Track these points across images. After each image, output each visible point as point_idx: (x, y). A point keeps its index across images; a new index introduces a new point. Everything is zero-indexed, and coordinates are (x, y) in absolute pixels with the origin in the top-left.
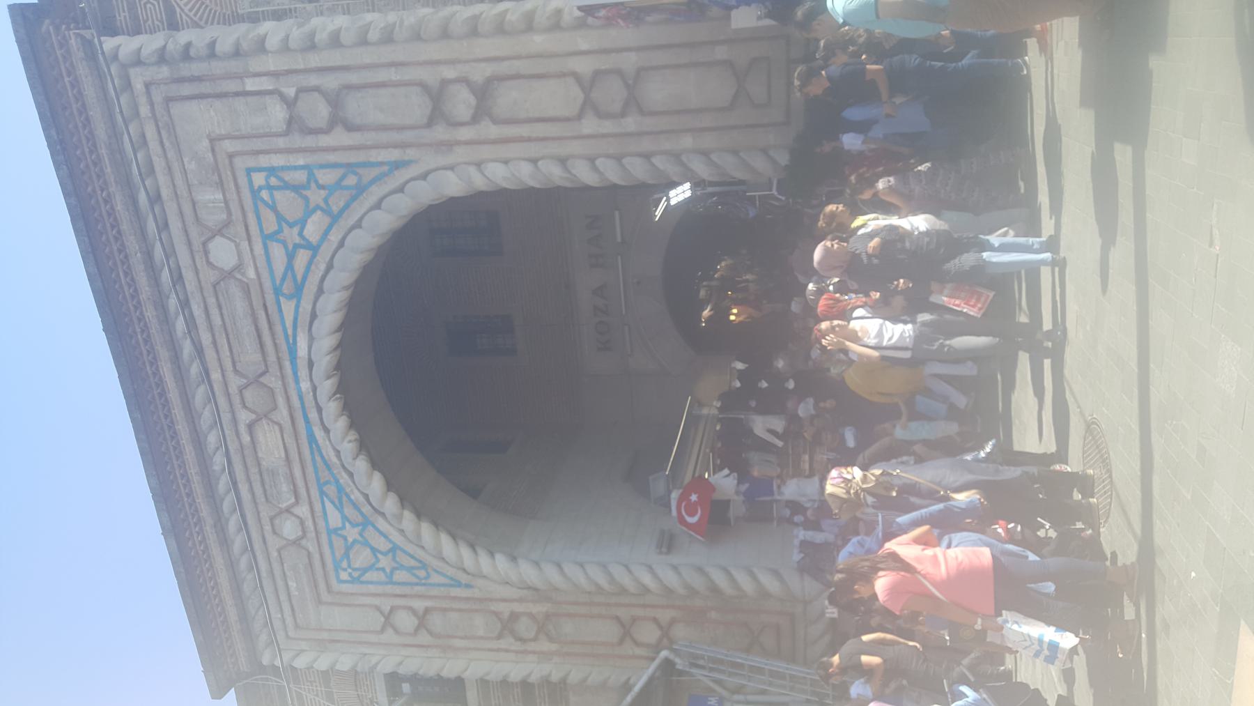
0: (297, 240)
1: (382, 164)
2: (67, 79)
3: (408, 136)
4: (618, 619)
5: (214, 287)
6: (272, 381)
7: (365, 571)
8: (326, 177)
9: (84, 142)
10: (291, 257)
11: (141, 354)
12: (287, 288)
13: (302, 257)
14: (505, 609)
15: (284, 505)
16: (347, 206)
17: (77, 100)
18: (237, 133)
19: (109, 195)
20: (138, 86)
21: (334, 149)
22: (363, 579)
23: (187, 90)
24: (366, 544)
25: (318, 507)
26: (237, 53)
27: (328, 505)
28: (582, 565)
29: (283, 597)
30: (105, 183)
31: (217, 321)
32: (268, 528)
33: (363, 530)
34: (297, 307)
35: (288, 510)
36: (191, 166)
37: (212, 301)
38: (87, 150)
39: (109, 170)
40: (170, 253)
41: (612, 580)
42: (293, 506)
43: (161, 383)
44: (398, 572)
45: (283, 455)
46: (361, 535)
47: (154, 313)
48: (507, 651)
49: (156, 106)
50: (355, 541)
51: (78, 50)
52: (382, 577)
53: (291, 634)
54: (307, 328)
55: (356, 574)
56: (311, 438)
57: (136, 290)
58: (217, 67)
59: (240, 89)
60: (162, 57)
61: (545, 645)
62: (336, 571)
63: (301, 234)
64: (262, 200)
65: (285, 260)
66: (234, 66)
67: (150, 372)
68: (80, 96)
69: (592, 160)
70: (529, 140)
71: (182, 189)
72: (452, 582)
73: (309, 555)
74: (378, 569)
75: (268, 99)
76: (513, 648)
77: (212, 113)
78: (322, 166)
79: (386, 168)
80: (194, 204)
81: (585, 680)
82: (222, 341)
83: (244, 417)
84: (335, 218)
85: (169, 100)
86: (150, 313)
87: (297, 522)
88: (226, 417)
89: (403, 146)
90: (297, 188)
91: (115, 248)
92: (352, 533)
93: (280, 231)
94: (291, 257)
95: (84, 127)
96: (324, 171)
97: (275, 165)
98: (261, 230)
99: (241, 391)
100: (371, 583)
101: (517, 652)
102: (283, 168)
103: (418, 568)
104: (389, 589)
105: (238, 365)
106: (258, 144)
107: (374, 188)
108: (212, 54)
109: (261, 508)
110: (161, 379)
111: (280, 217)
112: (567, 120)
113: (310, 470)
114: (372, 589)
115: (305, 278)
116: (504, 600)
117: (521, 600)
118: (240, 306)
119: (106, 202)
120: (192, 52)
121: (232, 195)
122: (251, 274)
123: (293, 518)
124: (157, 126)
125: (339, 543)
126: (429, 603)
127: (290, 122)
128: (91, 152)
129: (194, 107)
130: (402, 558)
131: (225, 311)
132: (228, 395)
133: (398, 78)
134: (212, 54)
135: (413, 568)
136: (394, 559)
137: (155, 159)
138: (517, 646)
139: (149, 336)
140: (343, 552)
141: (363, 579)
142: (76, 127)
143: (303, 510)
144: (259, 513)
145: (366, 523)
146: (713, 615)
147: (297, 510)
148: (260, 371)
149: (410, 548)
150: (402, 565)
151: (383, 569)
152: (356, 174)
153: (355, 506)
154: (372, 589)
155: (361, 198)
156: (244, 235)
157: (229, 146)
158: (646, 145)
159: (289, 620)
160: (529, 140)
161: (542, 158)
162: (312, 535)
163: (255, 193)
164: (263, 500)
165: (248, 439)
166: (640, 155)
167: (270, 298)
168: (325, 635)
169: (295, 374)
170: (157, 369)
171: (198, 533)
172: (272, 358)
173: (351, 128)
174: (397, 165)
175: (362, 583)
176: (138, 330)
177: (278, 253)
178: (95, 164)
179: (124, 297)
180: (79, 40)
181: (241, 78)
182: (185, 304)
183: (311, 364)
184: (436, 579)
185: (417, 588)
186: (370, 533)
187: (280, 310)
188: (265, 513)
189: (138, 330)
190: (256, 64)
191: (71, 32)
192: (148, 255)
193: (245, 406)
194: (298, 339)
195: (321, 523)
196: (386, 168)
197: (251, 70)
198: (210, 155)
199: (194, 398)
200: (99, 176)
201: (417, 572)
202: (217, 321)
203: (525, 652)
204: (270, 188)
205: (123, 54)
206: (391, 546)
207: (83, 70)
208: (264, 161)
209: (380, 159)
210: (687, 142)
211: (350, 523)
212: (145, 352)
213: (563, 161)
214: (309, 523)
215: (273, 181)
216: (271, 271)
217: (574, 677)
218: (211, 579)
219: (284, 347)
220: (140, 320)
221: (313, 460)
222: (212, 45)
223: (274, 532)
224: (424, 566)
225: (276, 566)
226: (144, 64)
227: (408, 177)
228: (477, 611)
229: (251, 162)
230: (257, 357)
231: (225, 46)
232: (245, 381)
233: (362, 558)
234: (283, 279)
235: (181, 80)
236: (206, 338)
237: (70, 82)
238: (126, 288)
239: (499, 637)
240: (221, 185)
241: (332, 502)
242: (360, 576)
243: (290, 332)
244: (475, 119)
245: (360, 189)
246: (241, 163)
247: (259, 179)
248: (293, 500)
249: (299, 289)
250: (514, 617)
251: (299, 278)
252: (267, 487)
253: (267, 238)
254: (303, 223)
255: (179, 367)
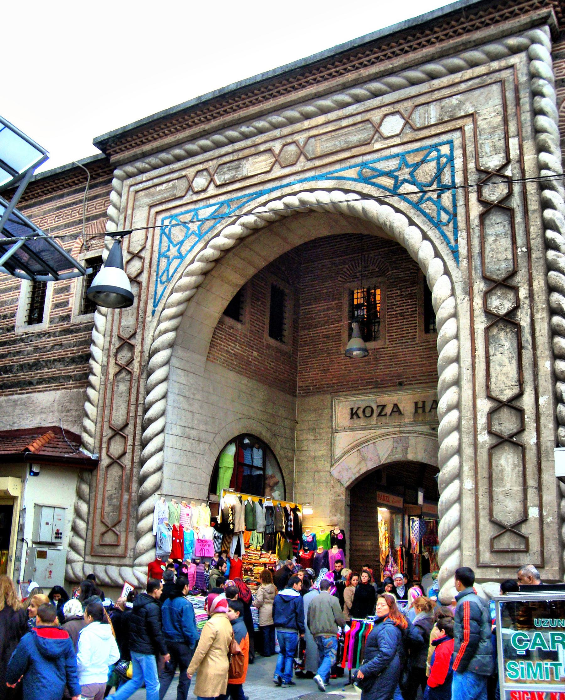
0: (401, 178)
1: (456, 241)
2: (516, 8)
3: (477, 262)
4: (126, 425)
5: (368, 120)
6: (302, 164)
7: (169, 238)
8: (446, 198)
9: (471, 23)
10: (388, 174)
11: (321, 72)
12: (367, 172)
13: (388, 182)
14: (136, 342)
15: (216, 178)
16: (425, 215)
17: (501, 16)
18: (478, 133)
19: (433, 43)
20: (514, 60)
21: (467, 205)
22: (164, 236)
23: (510, 95)
24: (186, 237)
25: (212, 201)
26: (537, 131)
27: (213, 209)
28: (164, 396)
29: (156, 181)
30: (442, 40)
31: (345, 123)
32: (200, 167)
33: (196, 234)
34: (353, 180)
35: (212, 180)
36: (454, 101)
37: (359, 118)
38: (465, 25)
39: (451, 42)
40: (394, 88)
41: (151, 421)
42: (215, 184)
43: (302, 87)
44: (166, 260)
45: (249, 174)
46: (192, 233)
47: (350, 79)
48: (110, 342)
49: (498, 73)
50: (188, 229)
51: (539, 15)
52: (164, 249)
53: (132, 189)
54: (337, 187)
55: (167, 231)
56: (261, 194)
57: (366, 66)
58: (526, 116)
59: (511, 134)
60: (534, 75)
61: (112, 370)
62: (169, 217)
63: (405, 181)
64: (430, 153)
65: (387, 170)
66: (528, 130)
67: (309, 79)
68: (505, 18)
69: (457, 406)
70: (473, 357)
71: (436, 95)
72: (157, 301)
73: (181, 197)
74: (169, 246)
75: (502, 155)
76: (112, 347)
77: (493, 114)
78: (454, 196)
79: (453, 243)
80: (428, 103)
81: (89, 400)
82: (330, 128)
83: (277, 146)
84: (416, 206)
85: (502, 82)
86: (350, 77)
87: (204, 187)
88: (277, 133)
89: (470, 257)
90: (438, 177)
91: (395, 49)
92: (194, 227)
93: (408, 166)
94: (388, 174)
95: (482, 23)
96: (451, 197)
97: (455, 161)
98: (408, 152)
99: (294, 142)
100: (161, 242)
101: (109, 350)
102: (453, 166)
103: (168, 275)
104: (156, 255)
105: (313, 140)
106: (470, 149)
107: (438, 233)
108: (537, 112)
109: (215, 161)
110: (304, 87)
111: (417, 165)
112: (488, 387)
113: (240, 194)
114: (157, 242)
115: (373, 184)
116: (143, 339)
117: (142, 352)
118: (354, 139)
119: (428, 41)
120: (537, 98)
121: (433, 131)
122: (377, 146)
123: (206, 184)
124: (484, 75)
125: (188, 217)
126: (144, 284)
127: (486, 172)
128: (464, 29)
129: (497, 100)
130: (175, 263)
131: (350, 128)
132: (292, 134)
133: (519, 253)
134: (537, 112)
135: (168, 271)
136: (175, 258)
137: (459, 75)
138: (113, 350)
139: (334, 76)
140: (182, 220)
141: (164, 236)
142: (481, 17)
143: (212, 191)
144: (211, 160)
145: (201, 236)
146: (126, 497)
147: (212, 186)
148: (308, 155)
149: (180, 270)
150: (170, 263)
151: (168, 250)
152: (449, 222)
153: (213, 228)
154: (157, 242)
155: (431, 226)
156: (405, 140)
157: (469, 128)
158: (468, 451)
159: (141, 186)
160: (473, 357)
161: (460, 367)
162: (195, 198)
163: (436, 147)
164: (220, 162)
165: (262, 150)
166: (460, 444)
167: (359, 160)
168: (129, 212)
169: (306, 180)
170: (312, 84)
171: (200, 120)
172: (318, 163)
173: (483, 217)
174: (455, 253)
175: (161, 236)
176: (338, 69)
177: (392, 165)
178: (455, 32)
179: (360, 58)
180: (546, 15)
181: (518, 135)
182: (358, 100)
183: (312, 190)
184: (160, 288)
185: (155, 274)
186: (194, 239)
187: (350, 167)
188: (211, 165)
189: (338, 69)
190: (529, 146)
191: (552, 9)
192: (391, 73)
193: (284, 145)
194: (330, 181)
195: (201, 204)
196: (453, 243)
197: (524, 142)
198: (463, 114)
199: (292, 110)
200: (446, 35)
201: (165, 274)
202: (345, 123)
203: (109, 356)
204: (439, 157)
205: (536, 48)
206: (183, 254)
207: (524, 19)
208: (458, 153)
209: (460, 239)
210: (469, 484)
211: (201, 225)
212: (322, 74)
213: (457, 382)
214: (203, 196)
215: (444, 160)
216: (379, 160)
217: (91, 392)
218: (170, 131)
219: (325, 171)
220: (345, 69)
221: (245, 196)
222: (542, 112)
223: (198, 172)
224: (169, 280)
225: (176, 175)
226: (529, 64)
227: (446, 258)
228: (137, 319)
229: (457, 143)
230: (319, 152)
231: (542, 121)
232: (302, 145)
233: (177, 234)
234: (373, 169)
235: (517, 90)
236: (332, 116)
237: (514, 11)
238: (367, 59)
239: (120, 338)
240: (441, 123)
241: (216, 211)
242: (165, 234)
243: (336, 175)
244: (488, 313)
245: (437, 224)
246: (456, 137)
247: (445, 150)
248: (218, 183)
249: (366, 180)
250: (132, 347)
251: (374, 180)
252: (228, 165)
253: (402, 156)
254: (413, 182)
255: (313, 99)
